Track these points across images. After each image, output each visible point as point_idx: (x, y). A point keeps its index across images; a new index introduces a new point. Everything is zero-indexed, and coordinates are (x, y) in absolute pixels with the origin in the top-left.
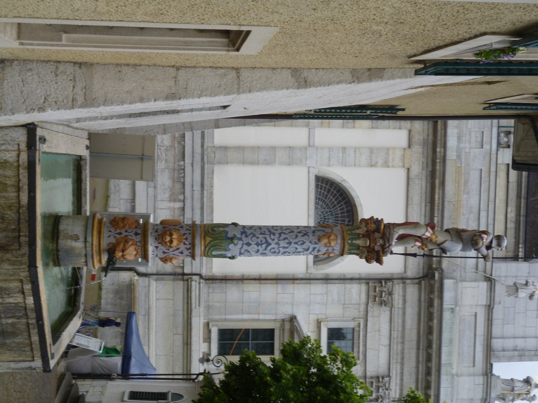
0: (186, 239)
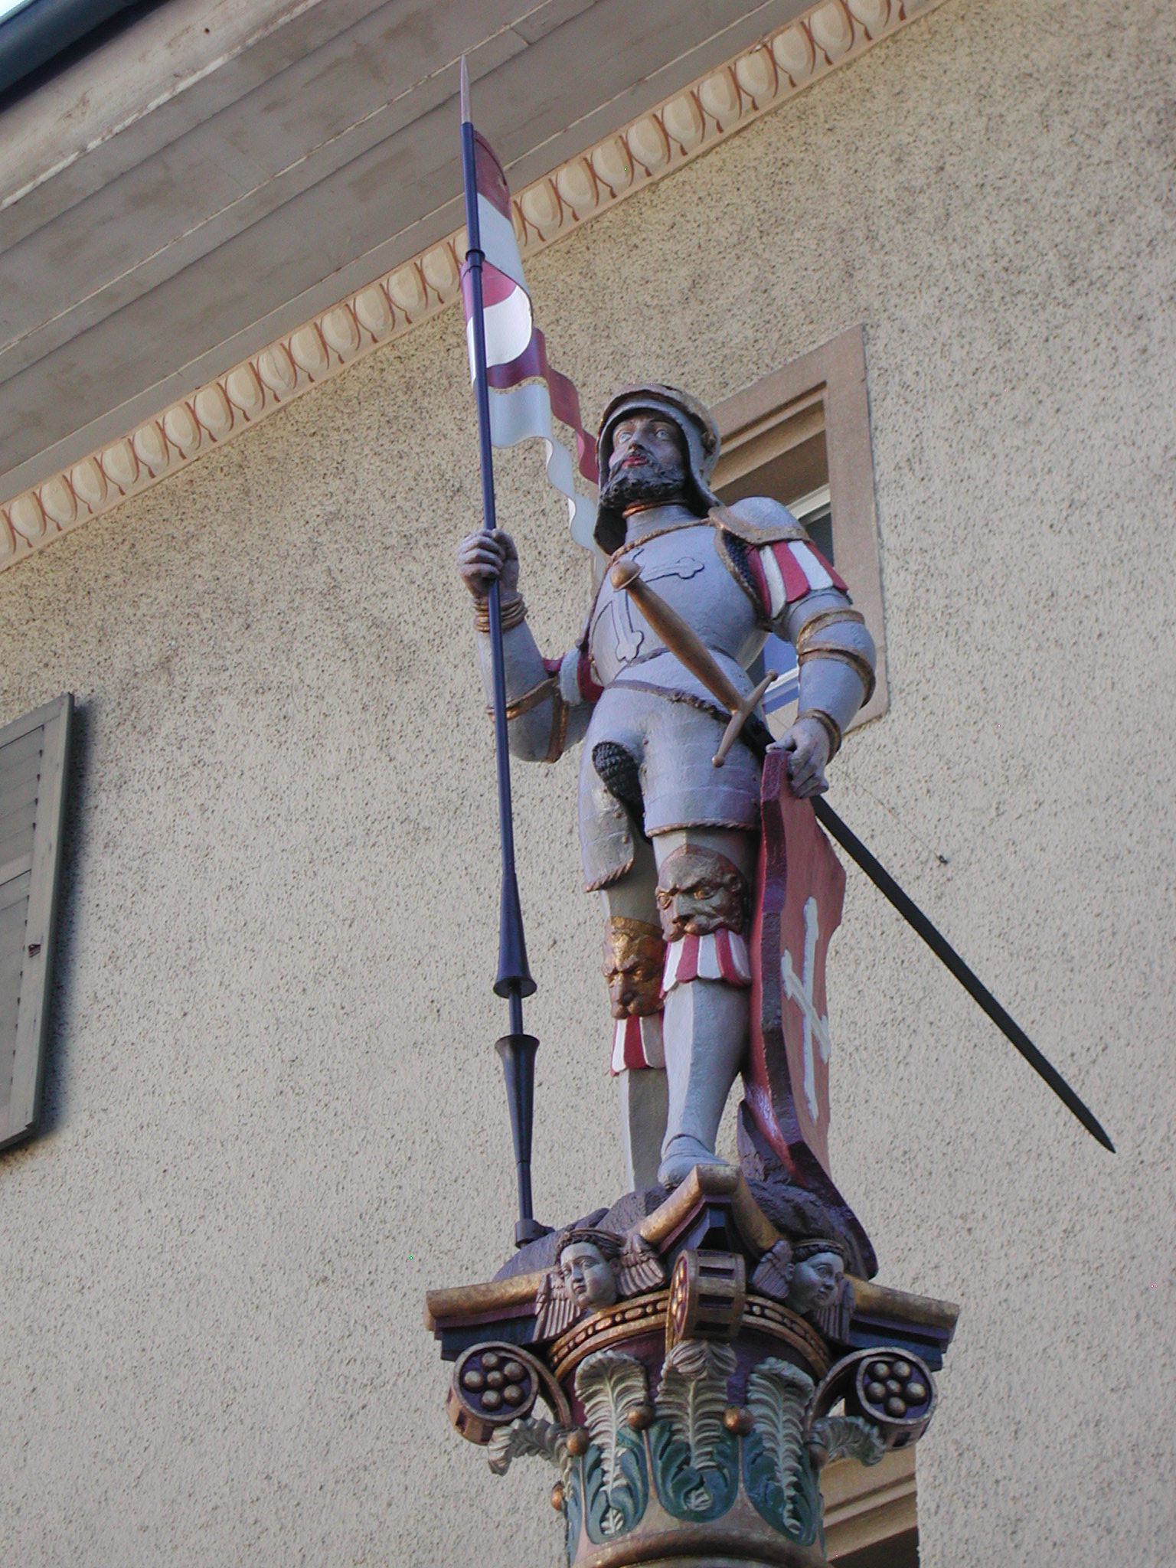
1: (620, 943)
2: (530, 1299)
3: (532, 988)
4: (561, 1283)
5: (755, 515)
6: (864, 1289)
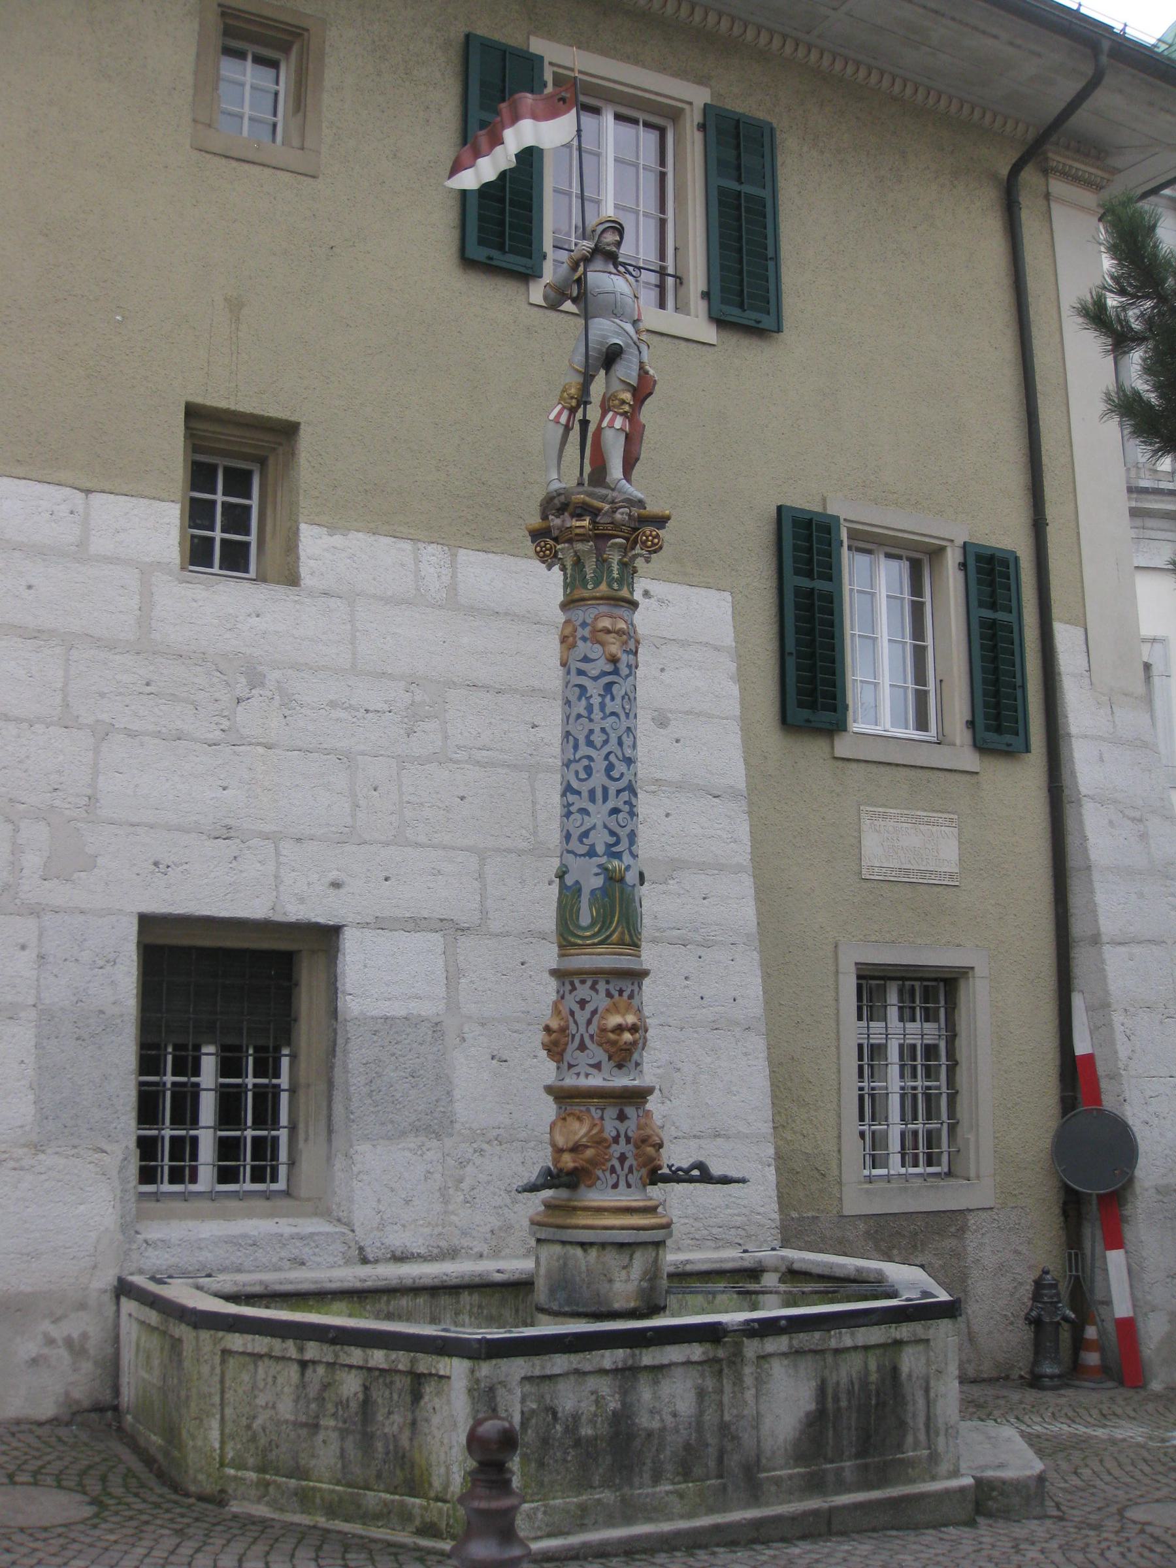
0: (621, 992)
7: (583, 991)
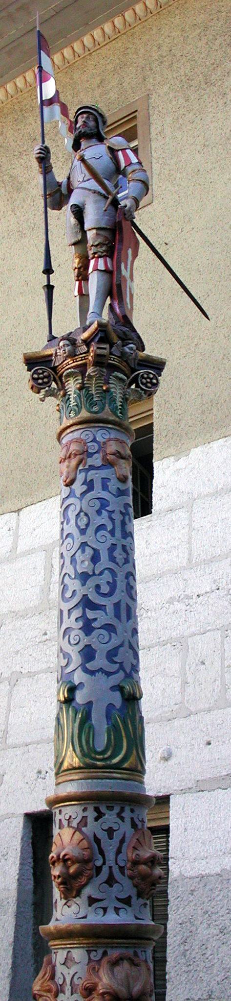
1: (77, 260)
2: (51, 355)
3: (53, 272)
4: (60, 351)
5: (117, 141)
6: (141, 354)
7: (110, 818)
